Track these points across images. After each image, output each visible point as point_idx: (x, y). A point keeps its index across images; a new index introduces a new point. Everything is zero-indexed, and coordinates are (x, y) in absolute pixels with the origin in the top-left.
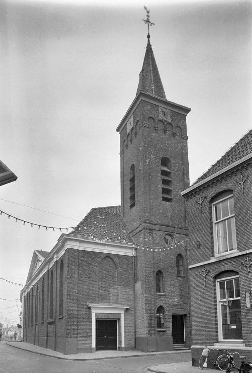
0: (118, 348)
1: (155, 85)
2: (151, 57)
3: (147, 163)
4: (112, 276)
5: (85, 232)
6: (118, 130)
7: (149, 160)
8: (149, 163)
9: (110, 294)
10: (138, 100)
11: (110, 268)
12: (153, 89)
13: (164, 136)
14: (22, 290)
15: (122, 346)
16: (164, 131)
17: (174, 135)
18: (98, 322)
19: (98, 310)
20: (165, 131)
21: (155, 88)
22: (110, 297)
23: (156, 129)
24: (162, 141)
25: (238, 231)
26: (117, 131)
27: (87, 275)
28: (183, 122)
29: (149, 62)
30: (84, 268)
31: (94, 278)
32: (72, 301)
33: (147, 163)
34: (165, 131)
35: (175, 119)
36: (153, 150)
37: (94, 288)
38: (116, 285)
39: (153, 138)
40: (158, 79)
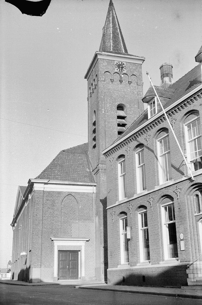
0: (79, 278)
1: (113, 41)
2: (112, 15)
3: (103, 112)
4: (74, 212)
5: (50, 175)
6: (85, 78)
7: (104, 109)
8: (105, 111)
9: (71, 228)
10: (88, 74)
11: (72, 204)
12: (112, 45)
13: (120, 86)
14: (104, 28)
15: (82, 276)
16: (120, 81)
17: (130, 83)
18: (59, 251)
19: (60, 244)
20: (121, 81)
21: (113, 44)
22: (71, 230)
23: (112, 81)
24: (118, 90)
25: (151, 217)
26: (85, 78)
27: (51, 212)
28: (139, 70)
29: (110, 20)
30: (49, 206)
31: (56, 214)
32: (37, 235)
33: (103, 112)
34: (121, 81)
35: (131, 69)
36: (109, 100)
37: (57, 223)
38: (77, 220)
39: (109, 89)
40: (117, 34)
